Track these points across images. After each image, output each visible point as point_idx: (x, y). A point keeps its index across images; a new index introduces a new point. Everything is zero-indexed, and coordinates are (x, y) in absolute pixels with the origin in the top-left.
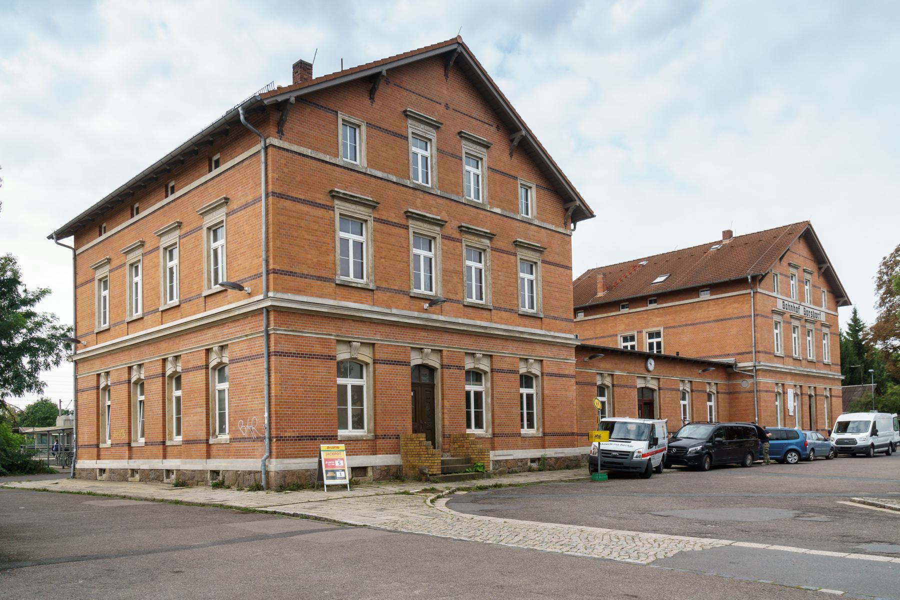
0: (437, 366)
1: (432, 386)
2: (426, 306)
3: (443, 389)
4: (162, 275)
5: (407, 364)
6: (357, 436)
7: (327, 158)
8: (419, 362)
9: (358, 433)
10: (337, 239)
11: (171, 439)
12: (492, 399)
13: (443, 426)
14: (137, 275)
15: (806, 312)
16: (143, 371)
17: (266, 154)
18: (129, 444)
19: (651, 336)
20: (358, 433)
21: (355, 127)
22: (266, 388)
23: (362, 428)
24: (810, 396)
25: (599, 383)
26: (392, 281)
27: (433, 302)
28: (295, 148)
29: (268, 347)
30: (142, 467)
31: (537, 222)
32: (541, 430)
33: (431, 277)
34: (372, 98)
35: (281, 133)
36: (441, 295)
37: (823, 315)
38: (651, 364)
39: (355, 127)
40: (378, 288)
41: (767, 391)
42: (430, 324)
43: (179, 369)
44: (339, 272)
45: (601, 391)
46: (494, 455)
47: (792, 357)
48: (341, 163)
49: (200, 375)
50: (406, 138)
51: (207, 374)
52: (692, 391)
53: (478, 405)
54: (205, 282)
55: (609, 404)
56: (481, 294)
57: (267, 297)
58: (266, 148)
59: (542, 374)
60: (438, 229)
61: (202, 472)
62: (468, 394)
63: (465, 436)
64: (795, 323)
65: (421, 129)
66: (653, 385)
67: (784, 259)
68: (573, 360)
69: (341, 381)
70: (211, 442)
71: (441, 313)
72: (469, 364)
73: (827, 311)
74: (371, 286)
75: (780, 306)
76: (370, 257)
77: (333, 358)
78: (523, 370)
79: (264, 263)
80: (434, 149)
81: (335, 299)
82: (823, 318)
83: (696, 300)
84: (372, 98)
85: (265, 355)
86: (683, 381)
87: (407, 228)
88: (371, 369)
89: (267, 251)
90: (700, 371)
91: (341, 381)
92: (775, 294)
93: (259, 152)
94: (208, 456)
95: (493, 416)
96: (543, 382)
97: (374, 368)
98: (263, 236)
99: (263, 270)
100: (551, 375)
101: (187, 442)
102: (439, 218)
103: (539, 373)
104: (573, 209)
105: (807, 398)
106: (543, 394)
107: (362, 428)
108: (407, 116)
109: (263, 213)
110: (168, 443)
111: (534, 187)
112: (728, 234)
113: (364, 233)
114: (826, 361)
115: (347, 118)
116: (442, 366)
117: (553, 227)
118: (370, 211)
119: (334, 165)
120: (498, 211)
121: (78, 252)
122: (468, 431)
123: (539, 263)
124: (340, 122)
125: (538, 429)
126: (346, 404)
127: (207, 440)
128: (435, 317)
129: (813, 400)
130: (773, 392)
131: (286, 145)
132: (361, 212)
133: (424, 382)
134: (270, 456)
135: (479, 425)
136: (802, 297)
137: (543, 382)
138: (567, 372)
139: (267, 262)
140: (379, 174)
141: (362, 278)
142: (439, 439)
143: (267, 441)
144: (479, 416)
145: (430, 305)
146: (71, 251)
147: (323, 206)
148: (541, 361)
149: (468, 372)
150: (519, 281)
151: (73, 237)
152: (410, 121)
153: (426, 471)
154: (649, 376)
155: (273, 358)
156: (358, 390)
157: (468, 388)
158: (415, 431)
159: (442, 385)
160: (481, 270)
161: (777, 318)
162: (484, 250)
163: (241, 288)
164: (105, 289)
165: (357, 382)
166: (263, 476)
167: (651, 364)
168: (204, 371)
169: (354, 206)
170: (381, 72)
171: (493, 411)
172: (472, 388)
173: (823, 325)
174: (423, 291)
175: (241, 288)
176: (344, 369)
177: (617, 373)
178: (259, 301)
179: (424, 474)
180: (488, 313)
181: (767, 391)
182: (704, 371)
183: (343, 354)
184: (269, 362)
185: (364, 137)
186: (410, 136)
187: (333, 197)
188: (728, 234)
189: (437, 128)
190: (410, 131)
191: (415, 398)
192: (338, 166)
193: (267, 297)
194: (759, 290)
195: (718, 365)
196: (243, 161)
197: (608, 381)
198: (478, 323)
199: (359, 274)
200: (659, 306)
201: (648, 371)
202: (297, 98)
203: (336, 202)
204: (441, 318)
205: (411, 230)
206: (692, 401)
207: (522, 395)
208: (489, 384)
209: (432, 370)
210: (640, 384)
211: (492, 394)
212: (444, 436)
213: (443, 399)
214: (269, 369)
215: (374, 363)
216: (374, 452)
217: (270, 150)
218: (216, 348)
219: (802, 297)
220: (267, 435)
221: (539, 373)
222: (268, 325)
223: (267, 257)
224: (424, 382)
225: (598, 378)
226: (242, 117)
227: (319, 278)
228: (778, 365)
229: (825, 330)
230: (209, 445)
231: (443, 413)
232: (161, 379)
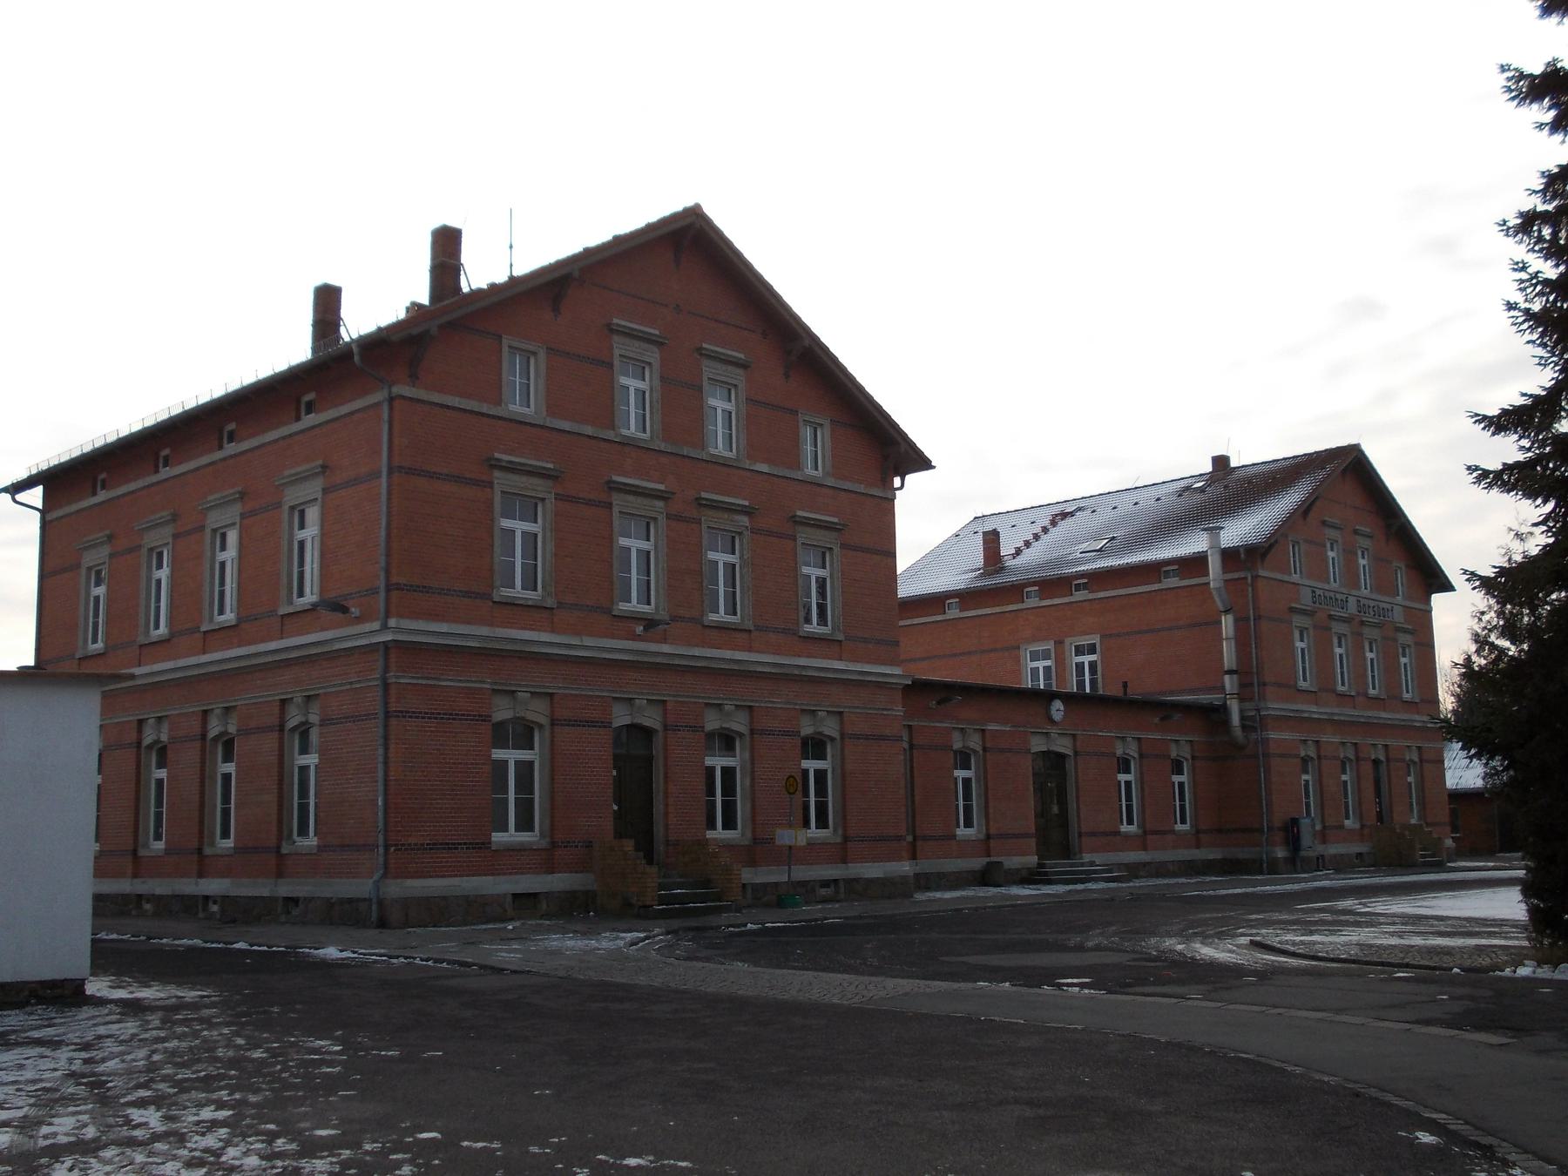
0: (657, 726)
1: (649, 760)
2: (639, 629)
3: (666, 765)
4: (207, 574)
5: (606, 725)
6: (522, 843)
7: (485, 408)
8: (626, 721)
9: (525, 837)
10: (497, 533)
11: (212, 844)
12: (753, 779)
13: (667, 826)
14: (160, 566)
15: (1361, 608)
16: (165, 727)
17: (391, 409)
18: (135, 852)
19: (1080, 651)
20: (525, 837)
21: (528, 354)
22: (380, 767)
23: (531, 829)
24: (1376, 762)
25: (957, 745)
26: (585, 589)
27: (650, 623)
28: (436, 397)
29: (386, 703)
30: (158, 891)
31: (830, 482)
32: (840, 832)
33: (648, 582)
34: (556, 310)
35: (414, 378)
36: (664, 615)
37: (1398, 610)
38: (1058, 705)
39: (528, 354)
40: (561, 605)
41: (1282, 756)
42: (646, 659)
43: (232, 729)
44: (498, 583)
45: (964, 760)
46: (748, 875)
47: (1334, 691)
48: (505, 415)
49: (270, 742)
50: (611, 366)
51: (281, 739)
52: (1141, 756)
53: (729, 789)
54: (284, 592)
55: (978, 781)
56: (735, 604)
57: (385, 627)
58: (391, 400)
59: (843, 735)
60: (660, 504)
61: (272, 900)
62: (710, 771)
63: (704, 843)
64: (1338, 628)
65: (634, 348)
66: (1063, 746)
67: (1312, 515)
68: (899, 710)
69: (498, 754)
70: (284, 851)
71: (664, 640)
72: (712, 723)
73: (1408, 603)
74: (550, 602)
75: (1306, 600)
76: (548, 556)
77: (486, 718)
78: (807, 730)
79: (382, 575)
80: (656, 375)
81: (491, 625)
82: (1398, 616)
83: (1156, 587)
84: (556, 310)
85: (381, 716)
86: (1123, 739)
87: (610, 506)
88: (547, 733)
89: (388, 555)
90: (1156, 720)
91: (498, 754)
92: (1295, 578)
93: (378, 405)
94: (280, 874)
95: (753, 808)
96: (842, 750)
97: (552, 733)
98: (383, 533)
99: (382, 584)
100: (857, 737)
101: (239, 850)
102: (662, 487)
103: (836, 735)
104: (897, 454)
105: (1367, 768)
106: (843, 769)
107: (531, 829)
108: (612, 331)
109: (384, 498)
110: (208, 851)
111: (827, 423)
112: (1221, 462)
113: (540, 520)
114: (1406, 696)
115: (515, 344)
116: (666, 727)
117: (862, 488)
118: (550, 483)
119: (494, 417)
120: (764, 468)
121: (49, 517)
122: (710, 834)
123: (836, 550)
124: (505, 350)
125: (835, 830)
126: (629, 572)
127: (279, 847)
128: (653, 647)
129: (1383, 768)
130: (1297, 756)
131: (422, 394)
132: (538, 486)
133: (635, 756)
134: (385, 876)
135: (729, 824)
136: (1352, 578)
137: (842, 750)
138: (887, 732)
139: (388, 571)
140: (566, 425)
141: (535, 589)
142: (660, 847)
143: (381, 850)
144: (729, 808)
145: (646, 629)
146: (38, 515)
147: (476, 483)
148: (841, 713)
149: (710, 736)
150: (800, 582)
151: (40, 488)
152: (616, 338)
153: (634, 901)
154: (1054, 731)
155: (393, 721)
156: (525, 769)
157: (709, 761)
158: (619, 835)
159: (666, 758)
160: (734, 566)
161: (1298, 620)
162: (740, 534)
163: (345, 610)
164: (98, 584)
165: (524, 755)
166: (374, 907)
167: (1058, 705)
168: (276, 735)
169: (524, 479)
170: (427, 331)
171: (753, 801)
172: (718, 762)
173: (1398, 629)
174: (634, 605)
175: (345, 610)
176: (501, 735)
177: (992, 727)
178: (369, 633)
179: (631, 905)
180: (745, 635)
181: (1282, 756)
182: (1162, 719)
183: (502, 711)
184: (386, 726)
185: (543, 367)
186: (616, 362)
187: (493, 467)
188: (1221, 462)
189: (660, 344)
190: (617, 352)
191: (619, 783)
192: (500, 418)
193: (385, 627)
194: (1262, 573)
195: (1187, 708)
196: (352, 413)
197: (975, 742)
198: (728, 654)
199: (530, 583)
200: (1091, 596)
201: (1052, 722)
202: (441, 327)
203: (497, 474)
204: (666, 648)
205: (616, 510)
206: (1142, 773)
207: (805, 772)
208: (747, 755)
209: (647, 733)
210: (1038, 745)
211: (753, 772)
212: (667, 843)
213: (666, 782)
214: (386, 738)
215: (552, 724)
216: (551, 870)
217: (396, 404)
218: (298, 700)
219: (1352, 578)
220: (381, 841)
221: (836, 735)
222: (386, 669)
223: (388, 564)
224: (635, 756)
225: (956, 736)
226: (356, 358)
227: (467, 594)
228: (1313, 710)
229: (1404, 639)
230: (281, 857)
231: (667, 805)
232: (198, 744)
